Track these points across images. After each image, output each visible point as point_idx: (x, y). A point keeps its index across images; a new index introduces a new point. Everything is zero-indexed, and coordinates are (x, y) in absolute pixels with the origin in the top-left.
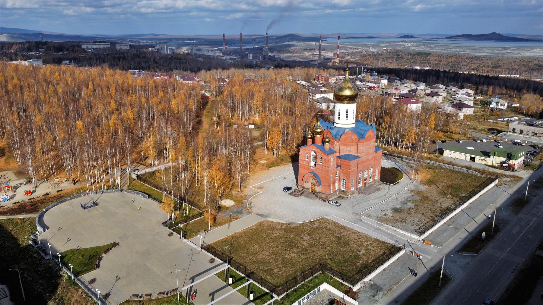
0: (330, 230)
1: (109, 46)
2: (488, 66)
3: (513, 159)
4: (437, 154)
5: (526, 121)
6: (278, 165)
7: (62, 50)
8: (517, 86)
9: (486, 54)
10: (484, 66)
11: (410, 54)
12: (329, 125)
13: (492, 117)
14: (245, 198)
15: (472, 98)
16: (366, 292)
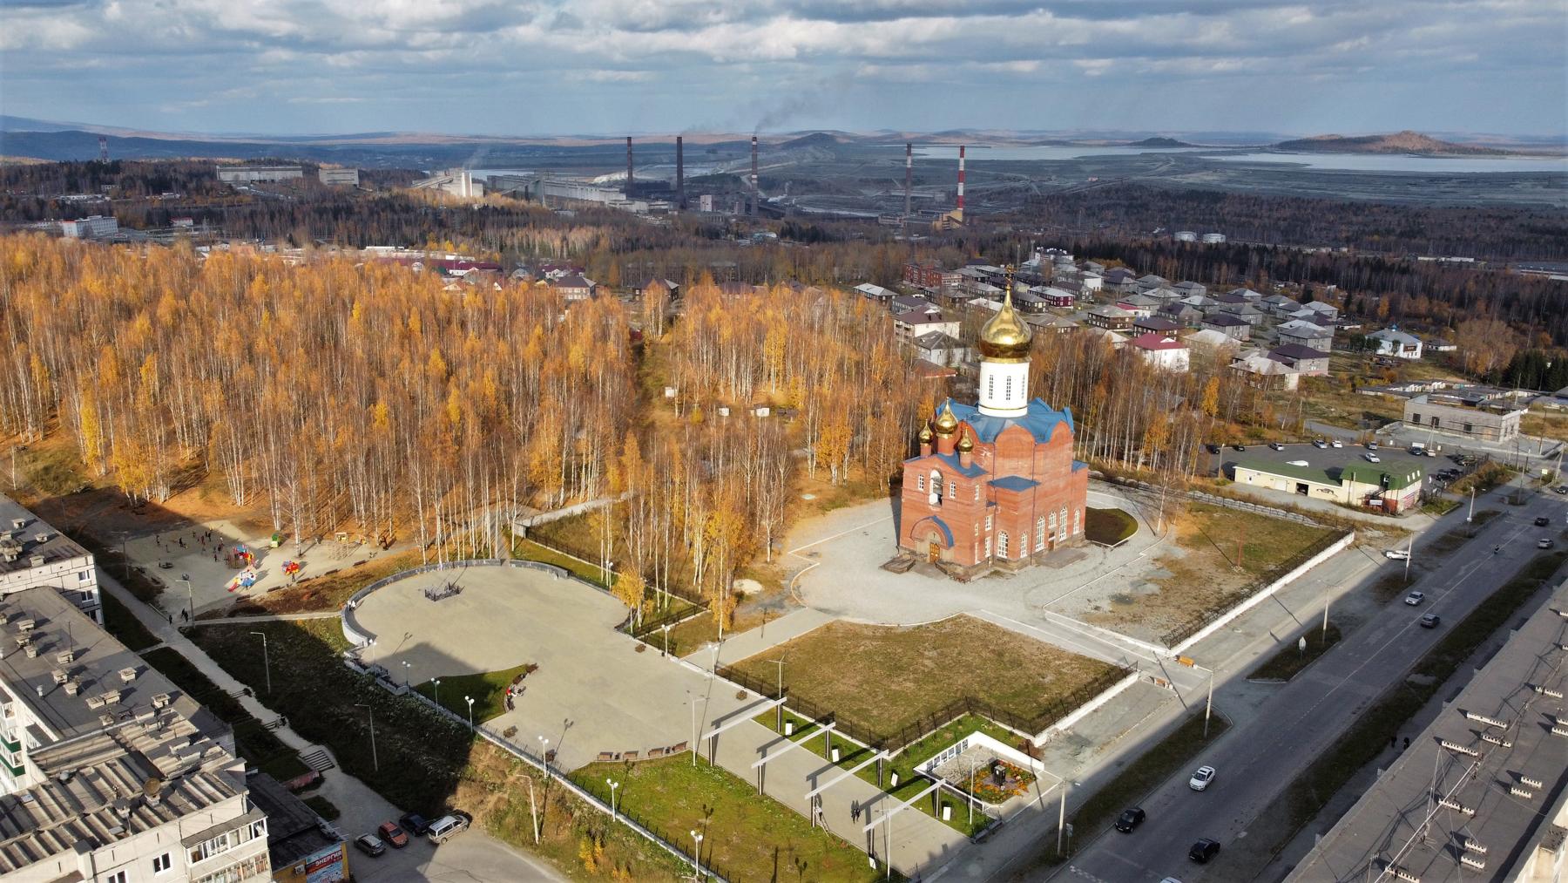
0: (979, 638)
1: (300, 174)
2: (1389, 232)
3: (1393, 488)
4: (1221, 477)
5: (1461, 392)
6: (844, 504)
7: (168, 188)
8: (1462, 292)
9: (1382, 197)
10: (1376, 232)
11: (1165, 195)
12: (968, 410)
13: (1374, 382)
14: (783, 577)
15: (1330, 330)
16: (1058, 749)
